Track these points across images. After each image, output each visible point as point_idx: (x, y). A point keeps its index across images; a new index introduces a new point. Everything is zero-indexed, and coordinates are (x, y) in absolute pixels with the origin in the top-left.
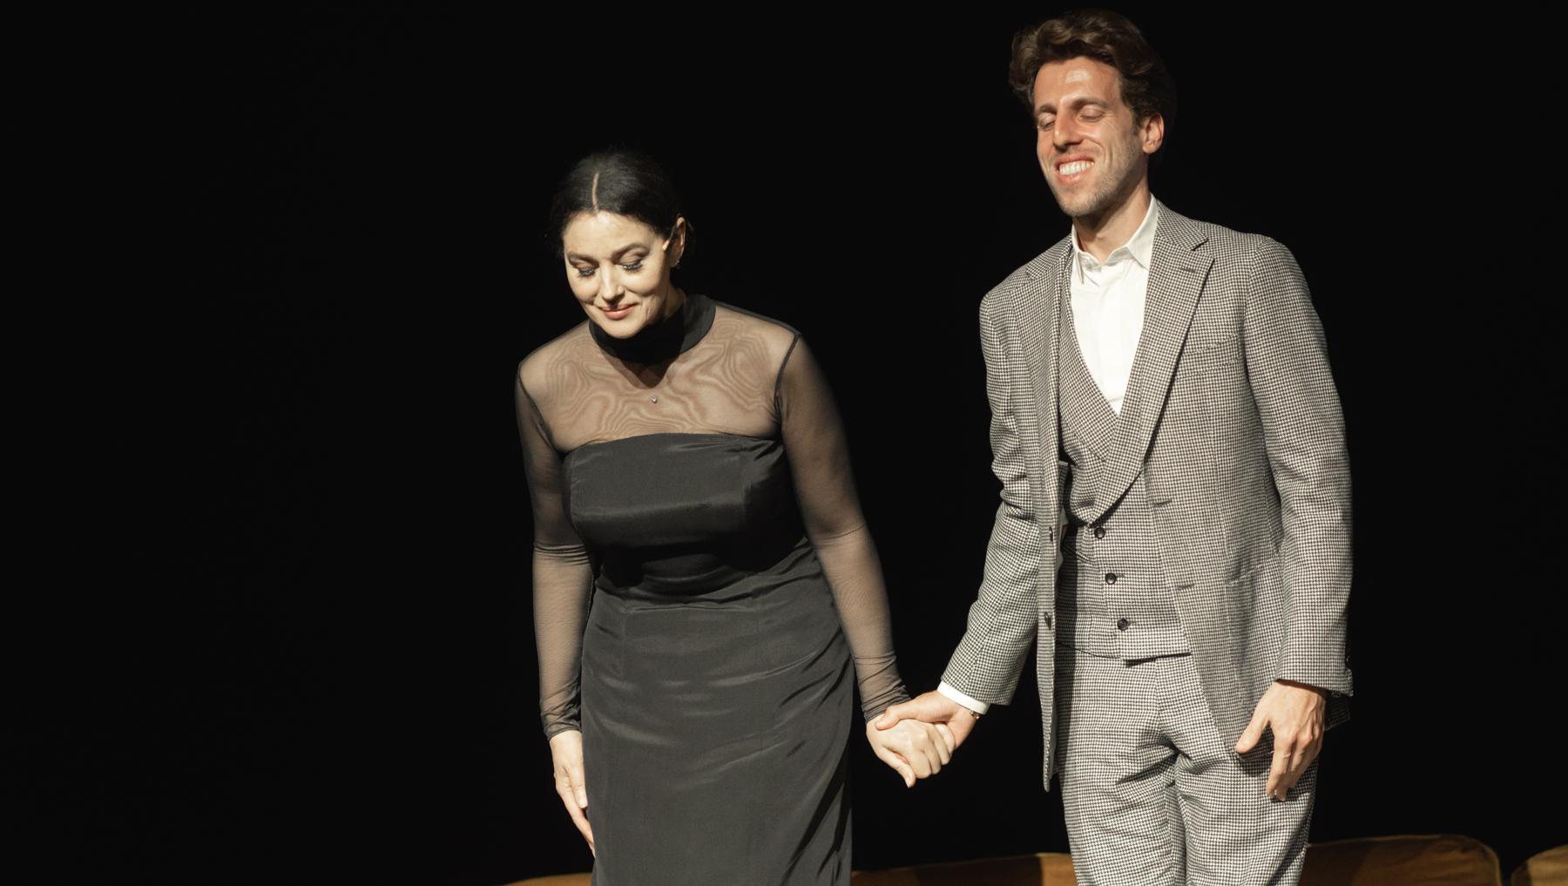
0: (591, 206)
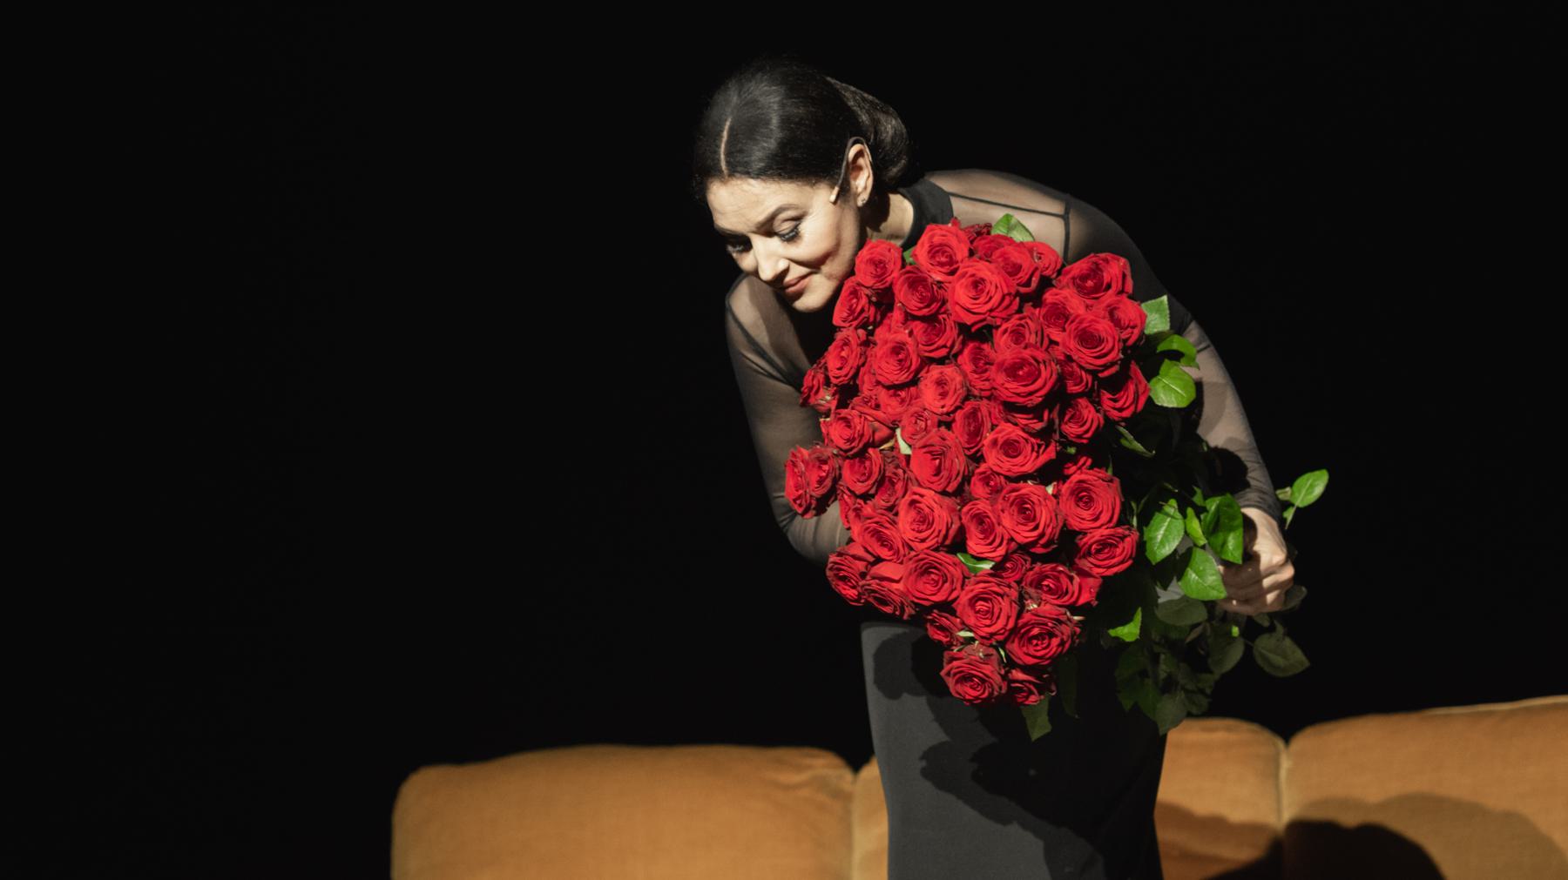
0: (721, 171)
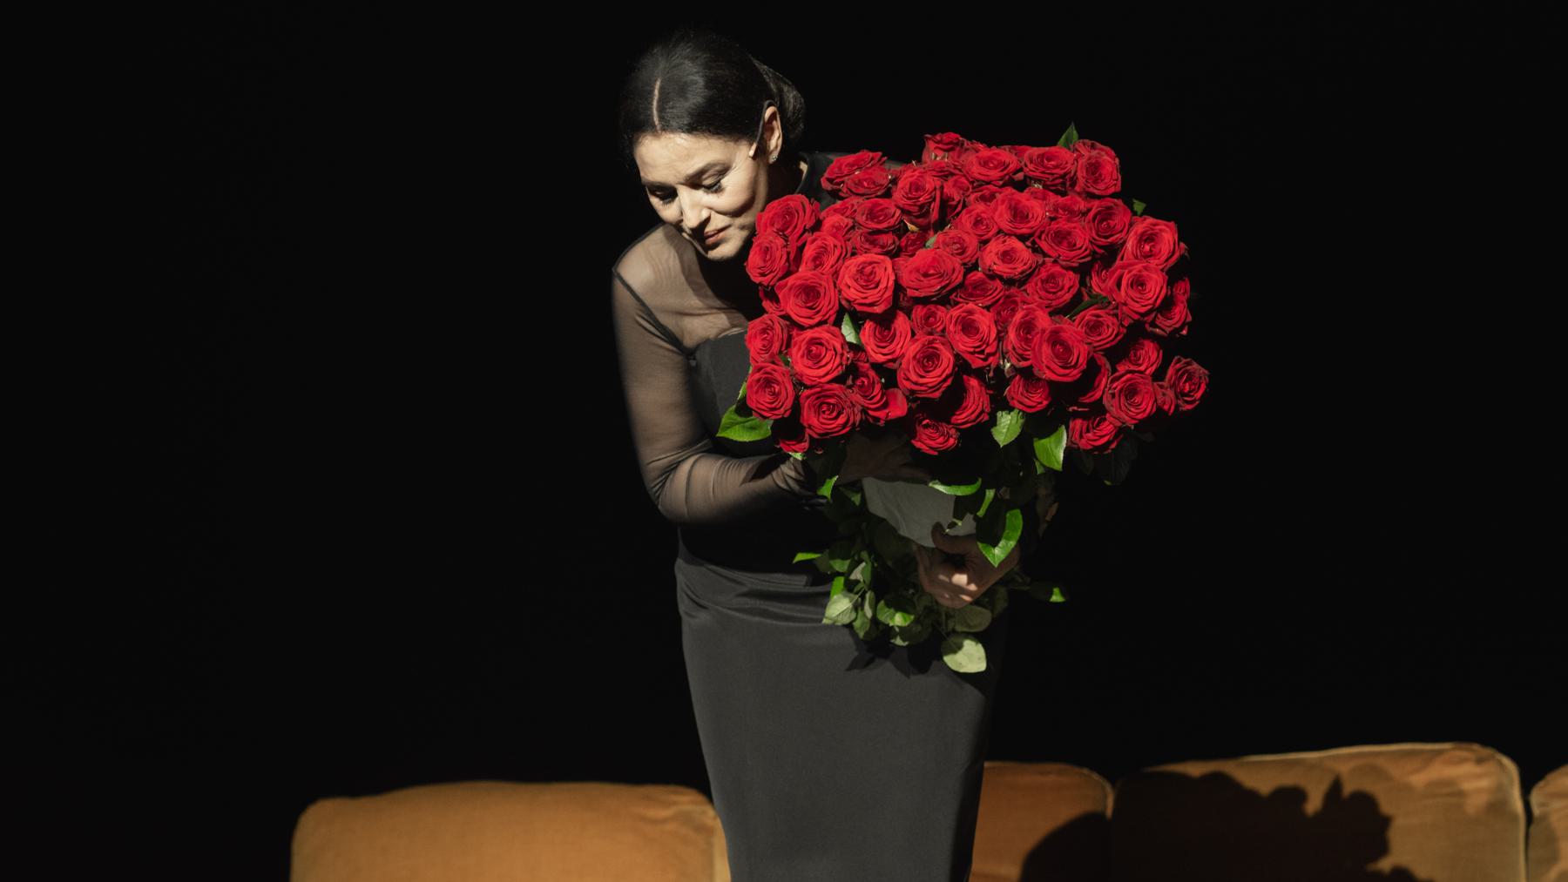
0: (654, 126)
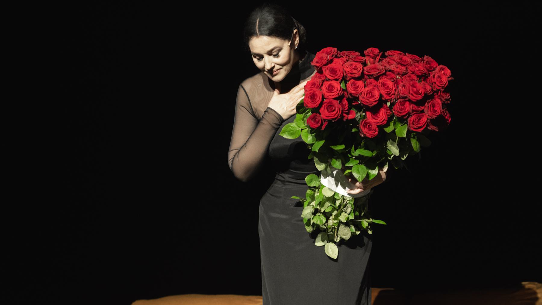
0: (256, 34)
